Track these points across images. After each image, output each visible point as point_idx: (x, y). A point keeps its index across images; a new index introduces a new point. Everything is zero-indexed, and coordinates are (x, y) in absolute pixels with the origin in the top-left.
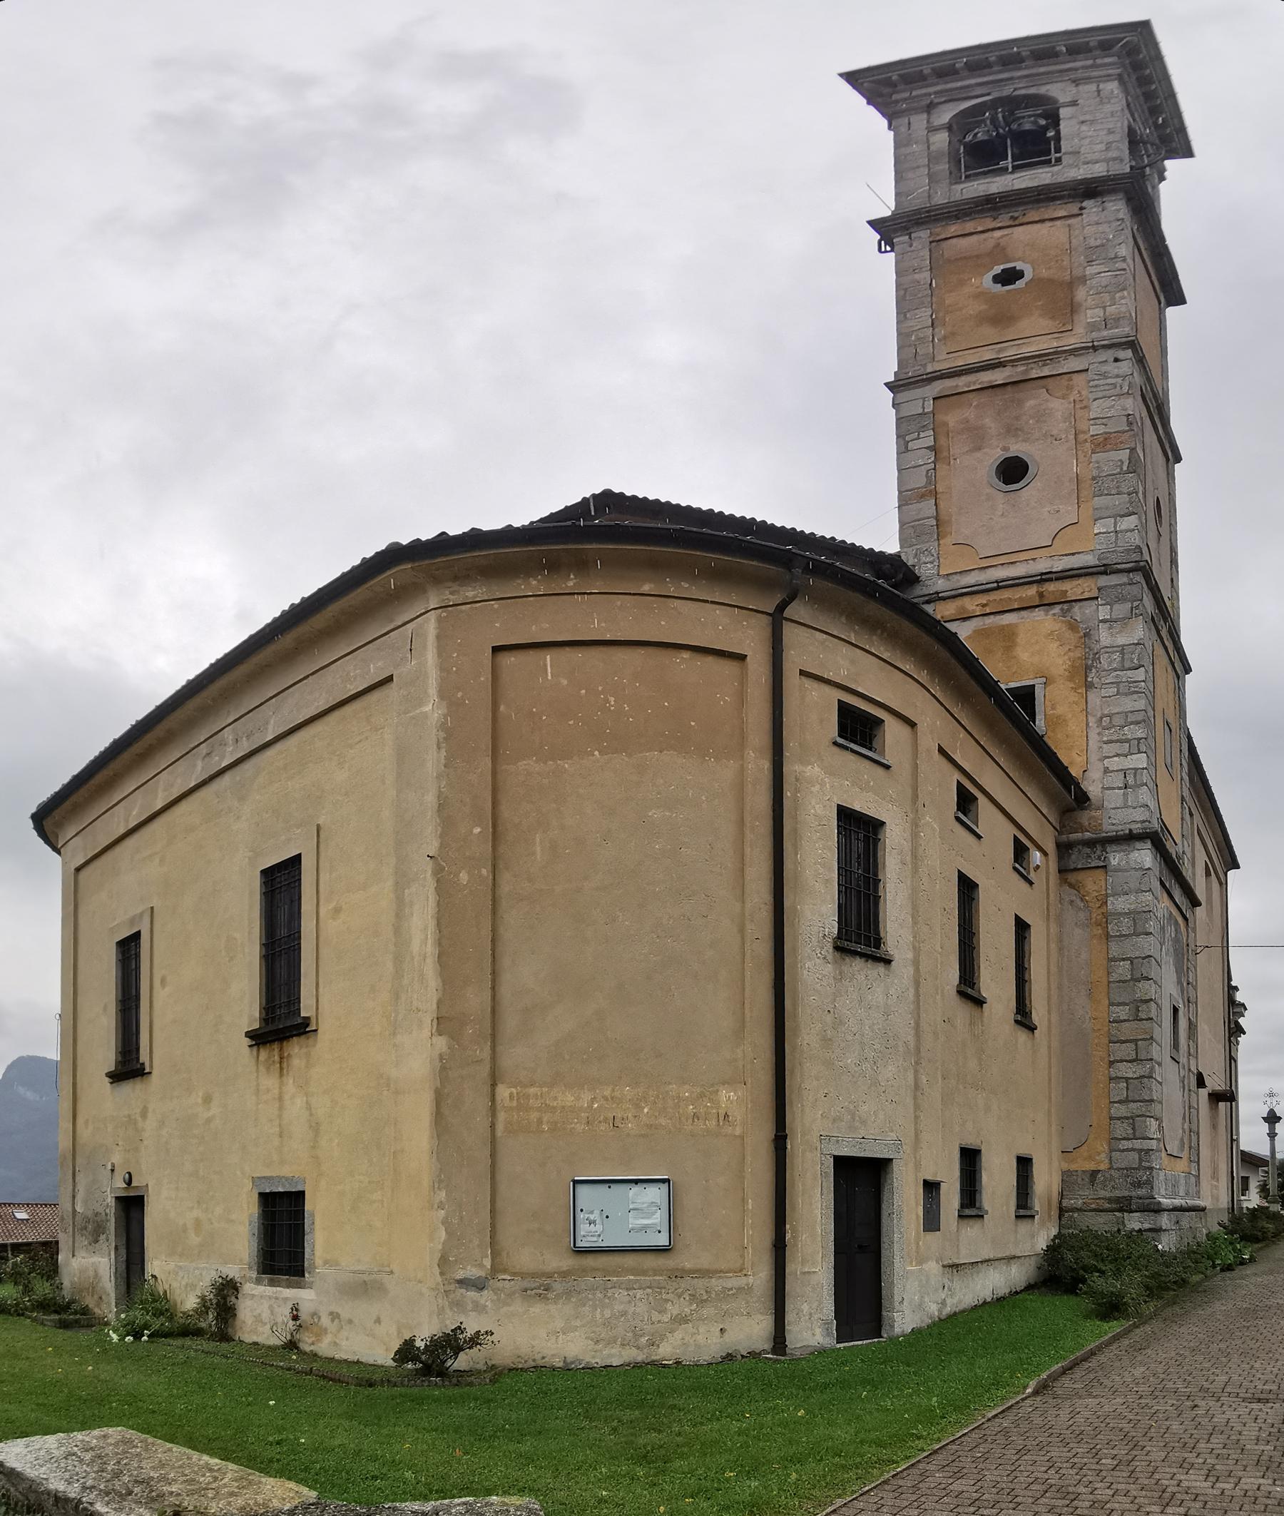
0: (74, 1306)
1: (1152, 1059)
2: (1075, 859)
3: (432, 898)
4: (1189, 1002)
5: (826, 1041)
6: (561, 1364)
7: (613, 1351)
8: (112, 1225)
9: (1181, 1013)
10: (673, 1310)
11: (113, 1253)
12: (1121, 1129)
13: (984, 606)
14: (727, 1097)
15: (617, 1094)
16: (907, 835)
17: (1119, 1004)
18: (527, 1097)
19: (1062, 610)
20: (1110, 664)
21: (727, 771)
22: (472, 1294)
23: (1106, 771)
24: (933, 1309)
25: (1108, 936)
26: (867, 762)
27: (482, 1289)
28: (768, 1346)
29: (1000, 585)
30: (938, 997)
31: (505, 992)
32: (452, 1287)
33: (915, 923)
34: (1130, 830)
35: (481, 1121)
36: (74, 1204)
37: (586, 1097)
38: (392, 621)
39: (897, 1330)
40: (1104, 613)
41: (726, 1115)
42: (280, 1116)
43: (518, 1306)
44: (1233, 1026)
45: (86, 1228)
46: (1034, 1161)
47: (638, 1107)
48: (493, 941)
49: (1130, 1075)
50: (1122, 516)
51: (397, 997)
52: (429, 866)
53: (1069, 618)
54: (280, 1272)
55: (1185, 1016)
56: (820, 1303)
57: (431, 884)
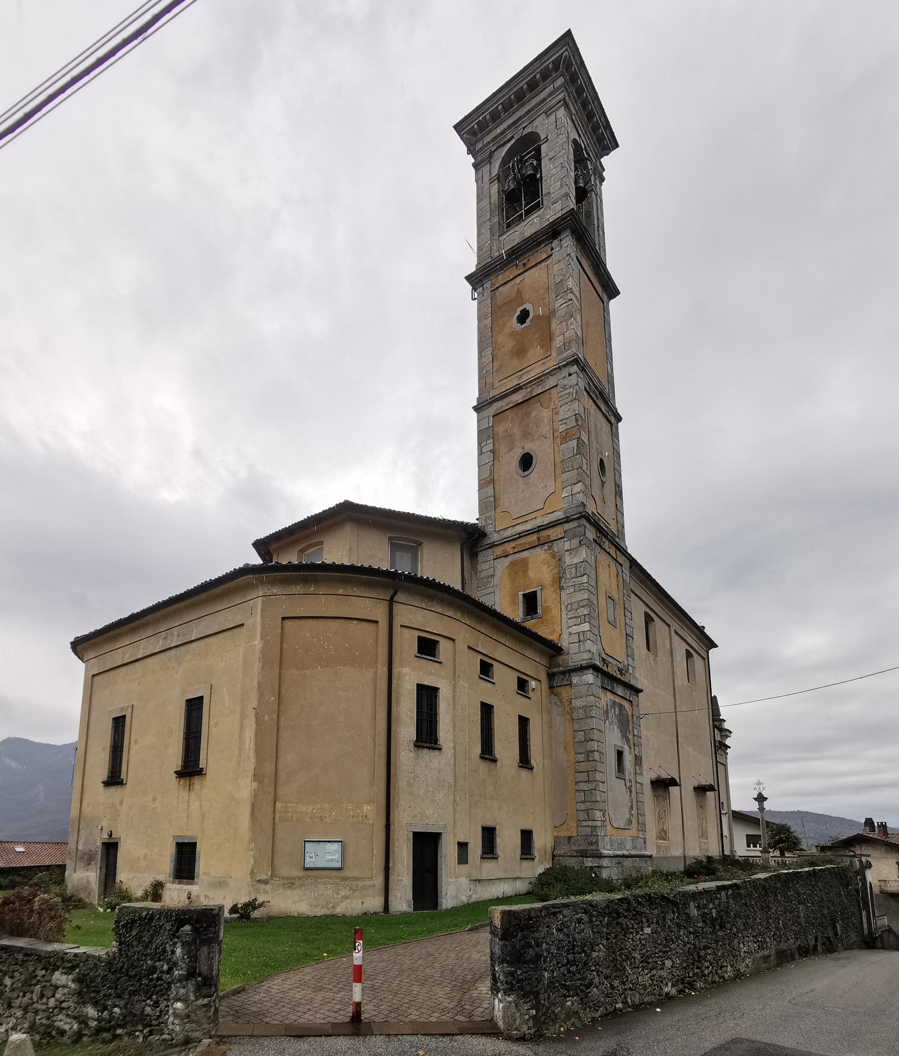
0: (74, 898)
3: (254, 726)
5: (410, 785)
7: (318, 910)
10: (343, 893)
11: (98, 872)
12: (582, 816)
14: (367, 808)
16: (451, 692)
17: (579, 754)
18: (288, 807)
19: (548, 546)
22: (263, 886)
24: (464, 899)
25: (573, 719)
27: (267, 884)
28: (382, 910)
32: (255, 883)
34: (581, 665)
36: (77, 845)
37: (310, 808)
38: (245, 598)
39: (444, 907)
42: (188, 809)
43: (281, 891)
45: (83, 858)
48: (277, 745)
49: (586, 789)
50: (574, 484)
52: (253, 712)
54: (184, 878)
55: (630, 753)
57: (254, 720)
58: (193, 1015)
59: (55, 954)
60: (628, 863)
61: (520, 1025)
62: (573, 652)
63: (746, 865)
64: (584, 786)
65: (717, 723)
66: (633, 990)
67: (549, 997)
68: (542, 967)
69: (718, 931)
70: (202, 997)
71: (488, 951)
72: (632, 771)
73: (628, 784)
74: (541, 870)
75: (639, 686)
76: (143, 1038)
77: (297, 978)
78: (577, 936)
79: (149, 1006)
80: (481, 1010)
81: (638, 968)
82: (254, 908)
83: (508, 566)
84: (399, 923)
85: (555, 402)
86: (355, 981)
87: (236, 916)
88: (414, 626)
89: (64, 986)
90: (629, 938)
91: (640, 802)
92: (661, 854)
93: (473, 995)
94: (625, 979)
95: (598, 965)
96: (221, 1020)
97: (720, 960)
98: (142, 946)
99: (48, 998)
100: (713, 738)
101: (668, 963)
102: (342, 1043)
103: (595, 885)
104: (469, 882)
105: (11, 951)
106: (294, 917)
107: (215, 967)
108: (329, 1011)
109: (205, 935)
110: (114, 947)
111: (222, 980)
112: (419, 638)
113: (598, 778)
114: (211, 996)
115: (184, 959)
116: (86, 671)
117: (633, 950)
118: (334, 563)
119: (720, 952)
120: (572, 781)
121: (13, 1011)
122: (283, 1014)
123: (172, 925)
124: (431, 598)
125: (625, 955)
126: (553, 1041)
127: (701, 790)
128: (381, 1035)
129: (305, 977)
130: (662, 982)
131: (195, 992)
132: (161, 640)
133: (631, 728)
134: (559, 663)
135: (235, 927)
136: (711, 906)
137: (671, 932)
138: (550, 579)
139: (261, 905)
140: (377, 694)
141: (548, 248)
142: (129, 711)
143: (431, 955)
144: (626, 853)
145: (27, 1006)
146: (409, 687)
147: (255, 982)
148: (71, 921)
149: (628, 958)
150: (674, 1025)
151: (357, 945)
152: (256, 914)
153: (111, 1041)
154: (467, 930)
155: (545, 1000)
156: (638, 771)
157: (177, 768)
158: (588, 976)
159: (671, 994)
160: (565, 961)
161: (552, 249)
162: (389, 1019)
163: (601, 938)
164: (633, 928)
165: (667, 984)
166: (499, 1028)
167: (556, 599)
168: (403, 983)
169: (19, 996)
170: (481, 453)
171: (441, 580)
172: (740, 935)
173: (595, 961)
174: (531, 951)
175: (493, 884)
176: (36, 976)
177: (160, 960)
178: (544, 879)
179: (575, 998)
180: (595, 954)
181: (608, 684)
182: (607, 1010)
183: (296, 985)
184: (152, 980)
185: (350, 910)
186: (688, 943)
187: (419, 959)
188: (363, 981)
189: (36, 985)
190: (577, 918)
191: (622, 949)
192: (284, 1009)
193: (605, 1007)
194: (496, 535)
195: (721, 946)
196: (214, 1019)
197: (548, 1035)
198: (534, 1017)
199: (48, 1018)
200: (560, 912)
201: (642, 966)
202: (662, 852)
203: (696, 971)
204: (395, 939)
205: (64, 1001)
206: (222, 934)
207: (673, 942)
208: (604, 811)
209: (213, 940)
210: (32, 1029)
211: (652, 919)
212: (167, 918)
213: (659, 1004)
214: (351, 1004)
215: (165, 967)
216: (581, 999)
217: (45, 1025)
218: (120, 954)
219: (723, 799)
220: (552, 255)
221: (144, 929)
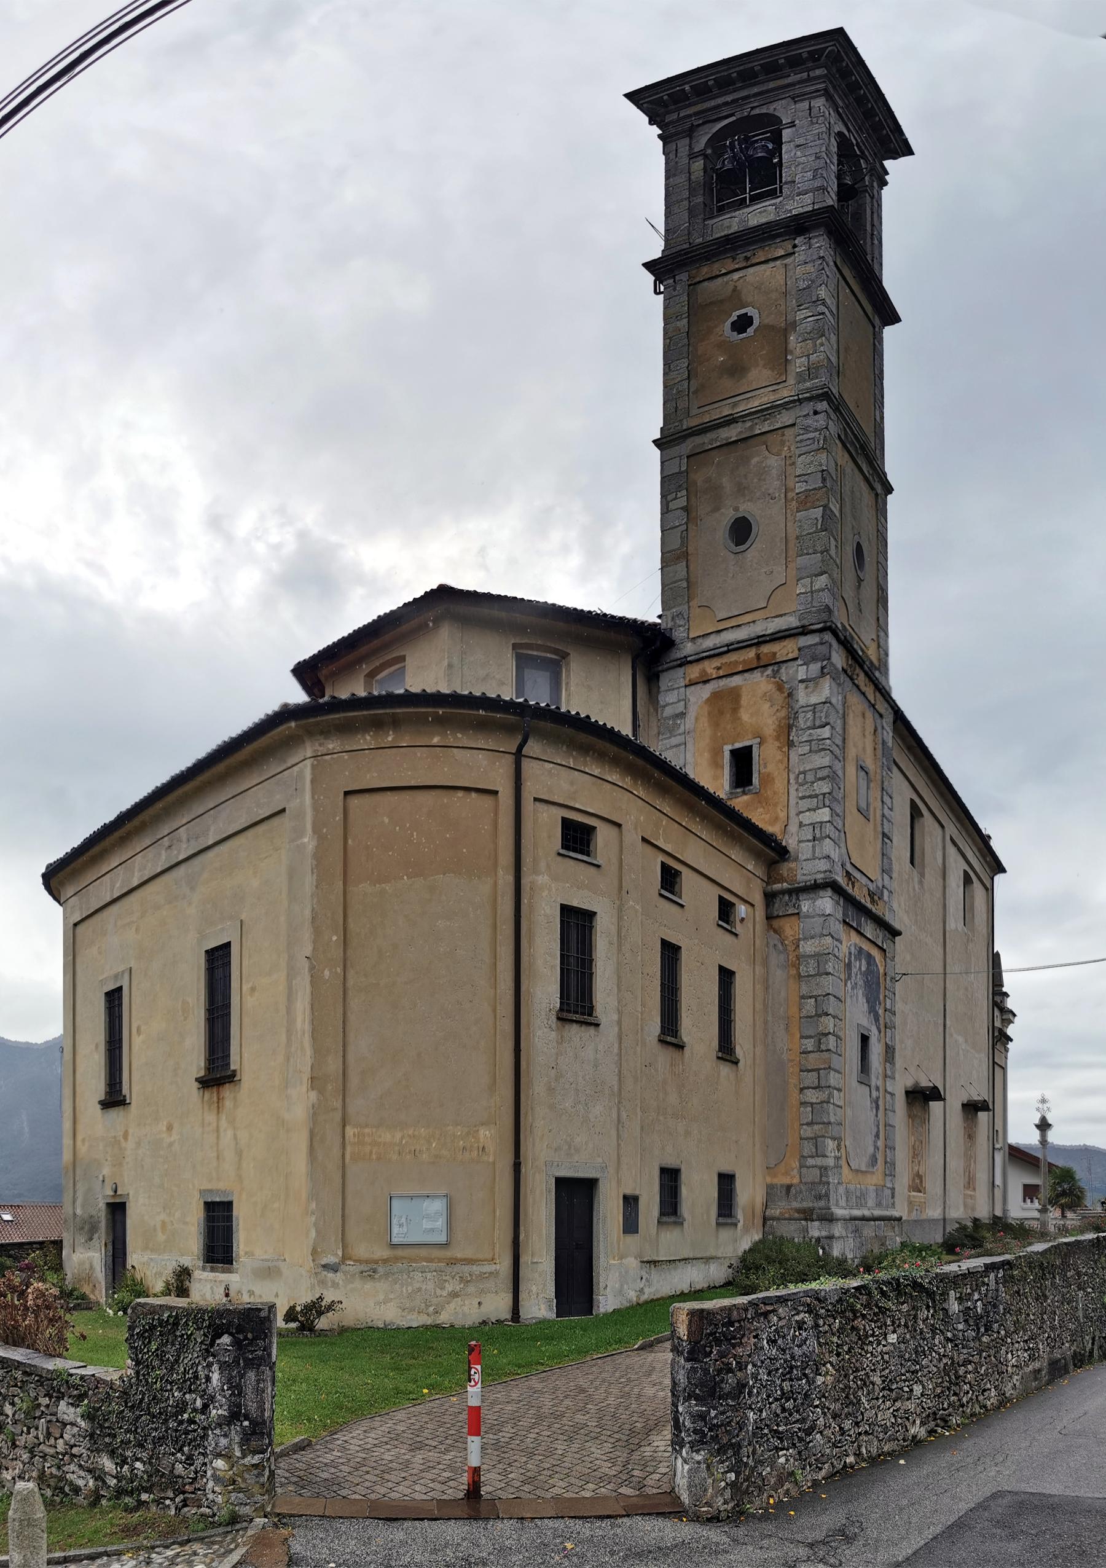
1: (829, 1087)
2: (778, 908)
4: (886, 1027)
5: (551, 1090)
6: (382, 1326)
7: (413, 1317)
8: (103, 1225)
9: (873, 1040)
10: (449, 1288)
12: (808, 1148)
13: (718, 668)
14: (485, 1134)
15: (416, 1133)
16: (615, 920)
19: (773, 670)
20: (805, 722)
21: (485, 888)
22: (331, 1275)
23: (801, 825)
24: (632, 1295)
25: (800, 976)
26: (582, 865)
27: (337, 1271)
28: (509, 1317)
29: (732, 648)
30: (638, 1049)
31: (351, 1058)
33: (619, 990)
34: (815, 880)
35: (336, 1152)
38: (285, 762)
40: (802, 673)
41: (484, 1148)
42: (217, 1144)
43: (357, 1284)
44: (996, 1034)
46: (737, 1176)
47: (429, 1143)
49: (814, 1101)
50: (816, 576)
51: (288, 1060)
52: (306, 964)
53: (777, 679)
55: (879, 1041)
56: (545, 1285)
58: (239, 1479)
59: (57, 1374)
60: (869, 1230)
61: (712, 1497)
62: (804, 858)
63: (1021, 1232)
64: (812, 1096)
65: (998, 999)
66: (869, 1434)
67: (754, 1452)
68: (745, 1403)
69: (983, 1335)
70: (251, 1452)
71: (668, 1382)
72: (880, 1071)
73: (875, 1094)
74: (745, 1245)
75: (897, 925)
76: (176, 1510)
77: (385, 1428)
78: (797, 1351)
79: (181, 1463)
80: (657, 1476)
81: (877, 1399)
82: (320, 1313)
83: (708, 700)
84: (535, 1339)
85: (789, 449)
86: (470, 1434)
87: (293, 1325)
88: (556, 799)
89: (73, 1424)
90: (867, 1352)
91: (890, 1125)
92: (914, 1216)
93: (646, 1454)
94: (860, 1418)
95: (824, 1396)
96: (279, 1490)
97: (982, 1380)
98: (166, 1368)
99: (56, 1439)
100: (991, 1023)
101: (918, 1389)
102: (454, 1531)
103: (822, 1267)
104: (639, 1264)
105: (9, 1366)
106: (378, 1328)
107: (267, 1406)
108: (433, 1481)
109: (252, 1352)
110: (127, 1366)
111: (278, 1428)
112: (564, 820)
113: (832, 1082)
114: (263, 1452)
115: (223, 1390)
116: (65, 918)
117: (872, 1371)
118: (424, 690)
119: (984, 1368)
120: (795, 1086)
121: (18, 1451)
122: (367, 1484)
123: (205, 1335)
124: (585, 750)
125: (861, 1380)
126: (759, 1519)
127: (972, 1108)
128: (511, 1518)
129: (398, 1427)
130: (908, 1419)
131: (241, 1445)
132: (163, 852)
133: (881, 997)
134: (781, 875)
135: (294, 1344)
136: (976, 1296)
137: (924, 1340)
138: (774, 727)
139: (330, 1308)
140: (498, 924)
141: (788, 246)
142: (126, 976)
143: (583, 1391)
144: (867, 1213)
145: (33, 1447)
146: (548, 911)
147: (325, 1433)
148: (73, 1326)
149: (865, 1384)
150: (922, 1482)
151: (472, 1372)
152: (322, 1323)
153: (136, 1509)
154: (637, 1350)
155: (748, 1457)
156: (889, 1073)
157: (198, 1073)
158: (809, 1416)
159: (918, 1438)
160: (779, 1392)
161: (795, 246)
162: (522, 1495)
163: (830, 1352)
164: (873, 1335)
165: (914, 1421)
166: (682, 1504)
167: (781, 761)
168: (541, 1438)
169: (23, 1432)
170: (665, 510)
171: (600, 717)
172: (1009, 1340)
173: (820, 1391)
174: (731, 1379)
175: (675, 1269)
176: (39, 1405)
177: (190, 1391)
178: (750, 1259)
179: (791, 1451)
180: (820, 1380)
181: (853, 917)
182: (833, 1467)
183: (385, 1439)
184: (181, 1422)
185: (460, 1316)
186: (944, 1356)
187: (566, 1397)
188: (482, 1433)
189: (40, 1418)
190: (797, 1321)
191: (857, 1370)
192: (367, 1477)
193: (832, 1464)
194: (690, 644)
195: (985, 1358)
196: (269, 1489)
197: (751, 1511)
198: (733, 1485)
199: (59, 1468)
200: (774, 1311)
201: (883, 1396)
202: (915, 1212)
203: (952, 1398)
204: (529, 1365)
205: (75, 1446)
206: (274, 1352)
207: (925, 1355)
208: (838, 1139)
209: (263, 1361)
210: (42, 1479)
211: (899, 1319)
212: (196, 1323)
213: (903, 1453)
214: (466, 1471)
215: (199, 1403)
216: (800, 1453)
217: (56, 1476)
218: (138, 1379)
219: (998, 1126)
220: (794, 253)
221: (167, 1341)
